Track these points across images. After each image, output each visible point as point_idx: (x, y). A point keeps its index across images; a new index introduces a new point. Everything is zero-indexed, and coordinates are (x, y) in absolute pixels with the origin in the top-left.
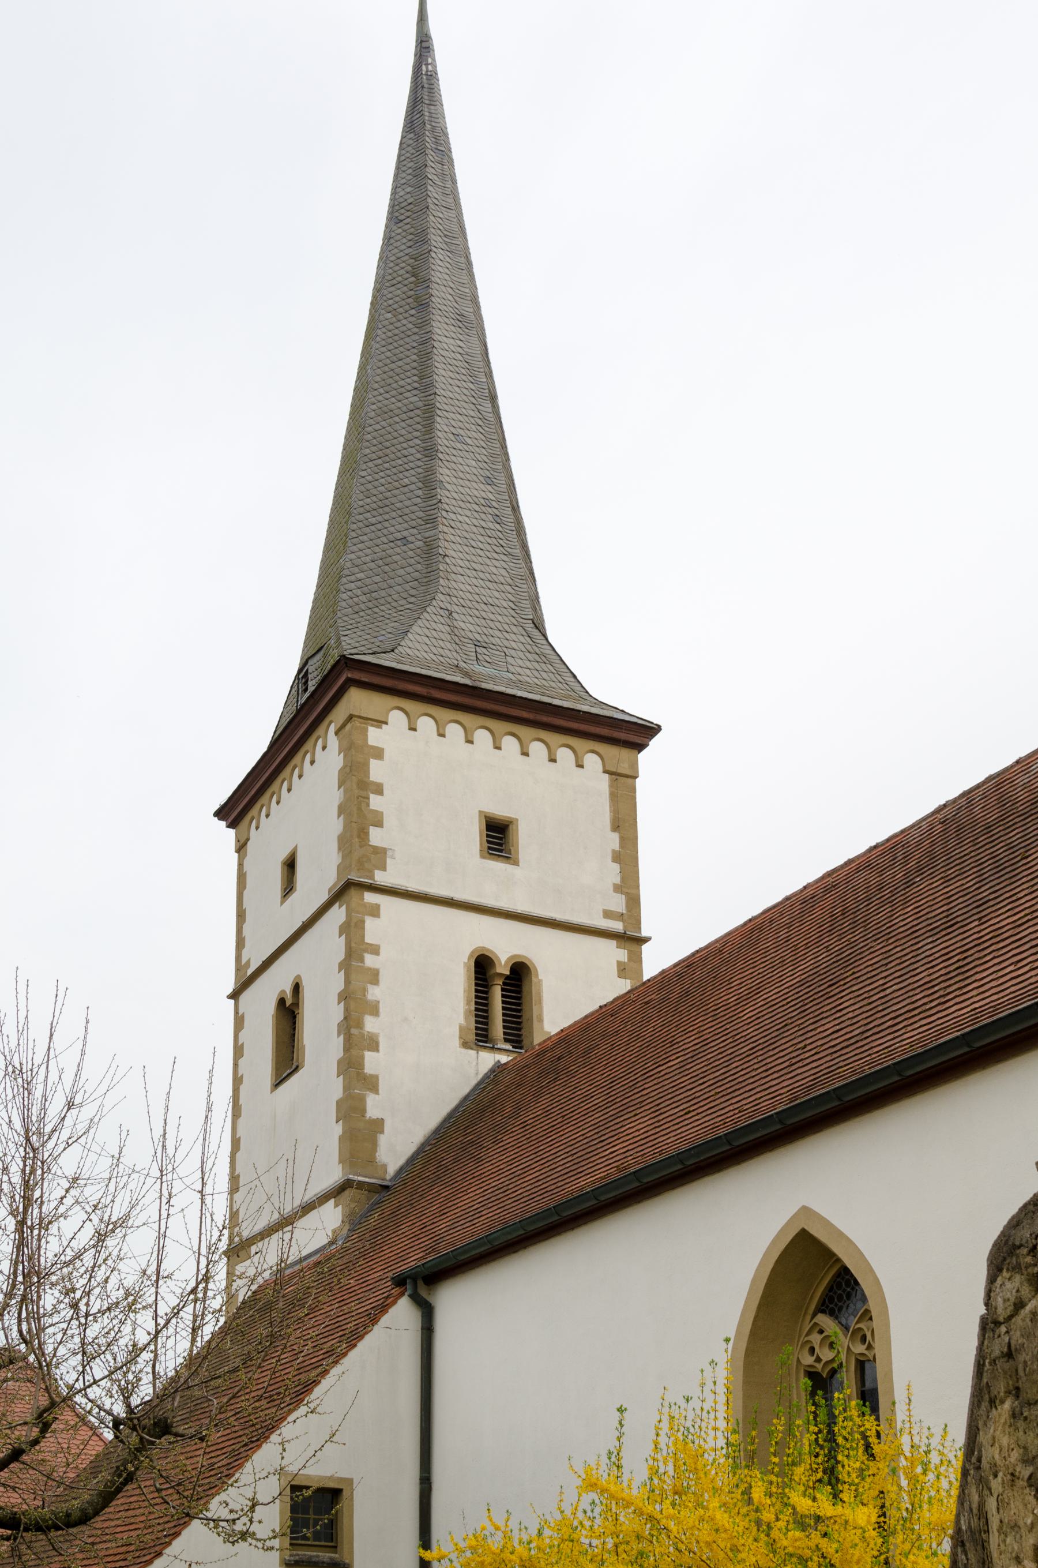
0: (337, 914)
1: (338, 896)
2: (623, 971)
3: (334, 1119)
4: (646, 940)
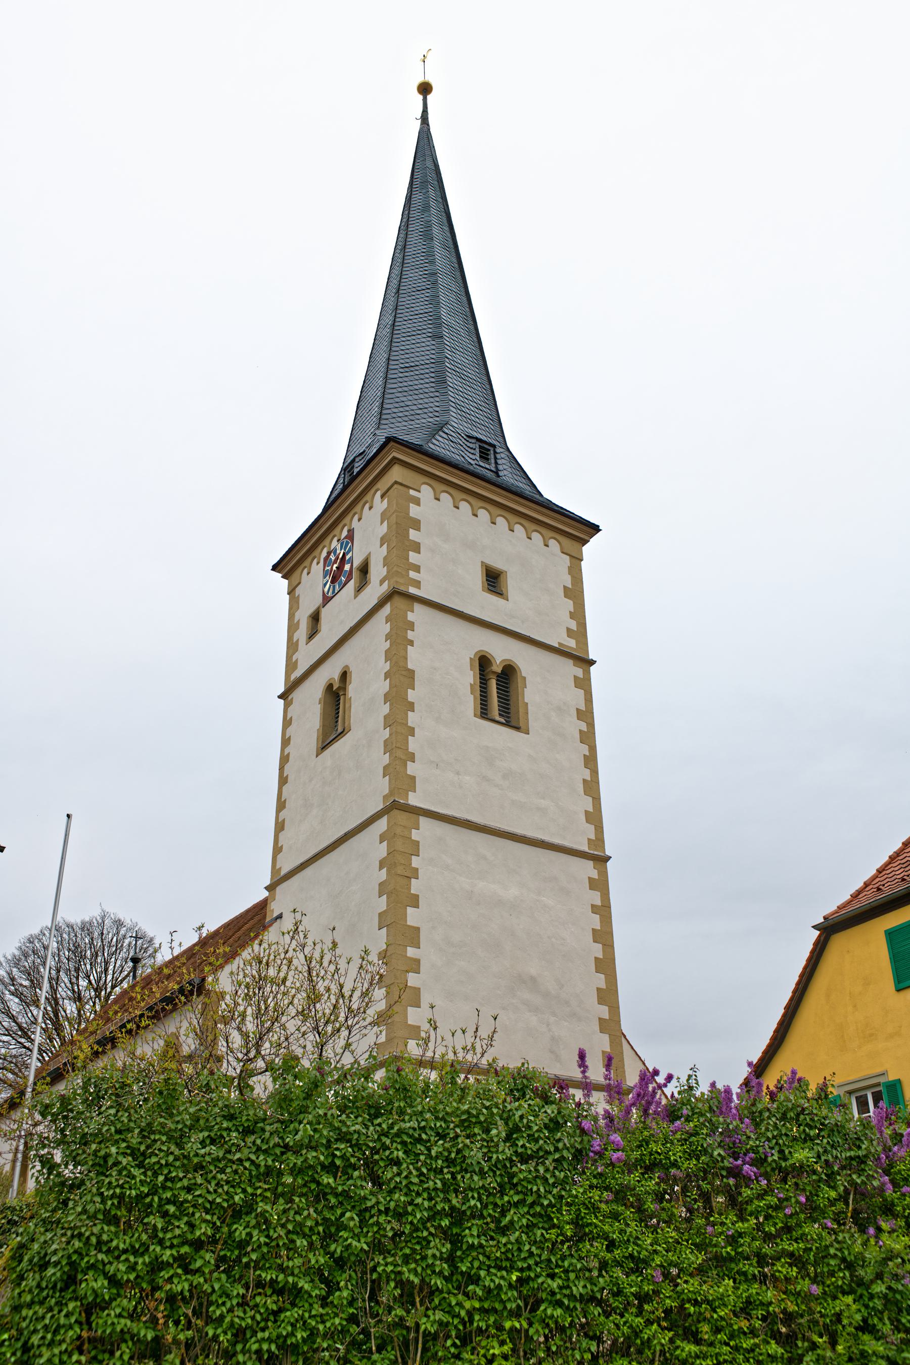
4: (592, 662)
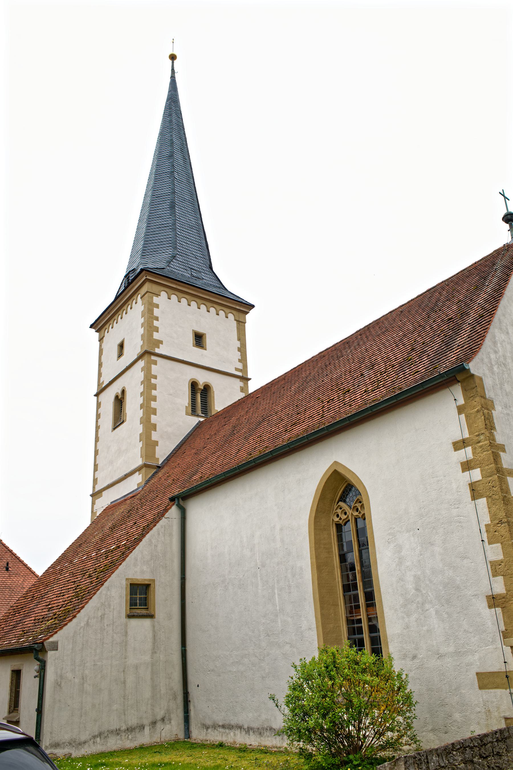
0: (141, 363)
1: (140, 357)
2: (242, 390)
3: (139, 441)
4: (250, 379)
